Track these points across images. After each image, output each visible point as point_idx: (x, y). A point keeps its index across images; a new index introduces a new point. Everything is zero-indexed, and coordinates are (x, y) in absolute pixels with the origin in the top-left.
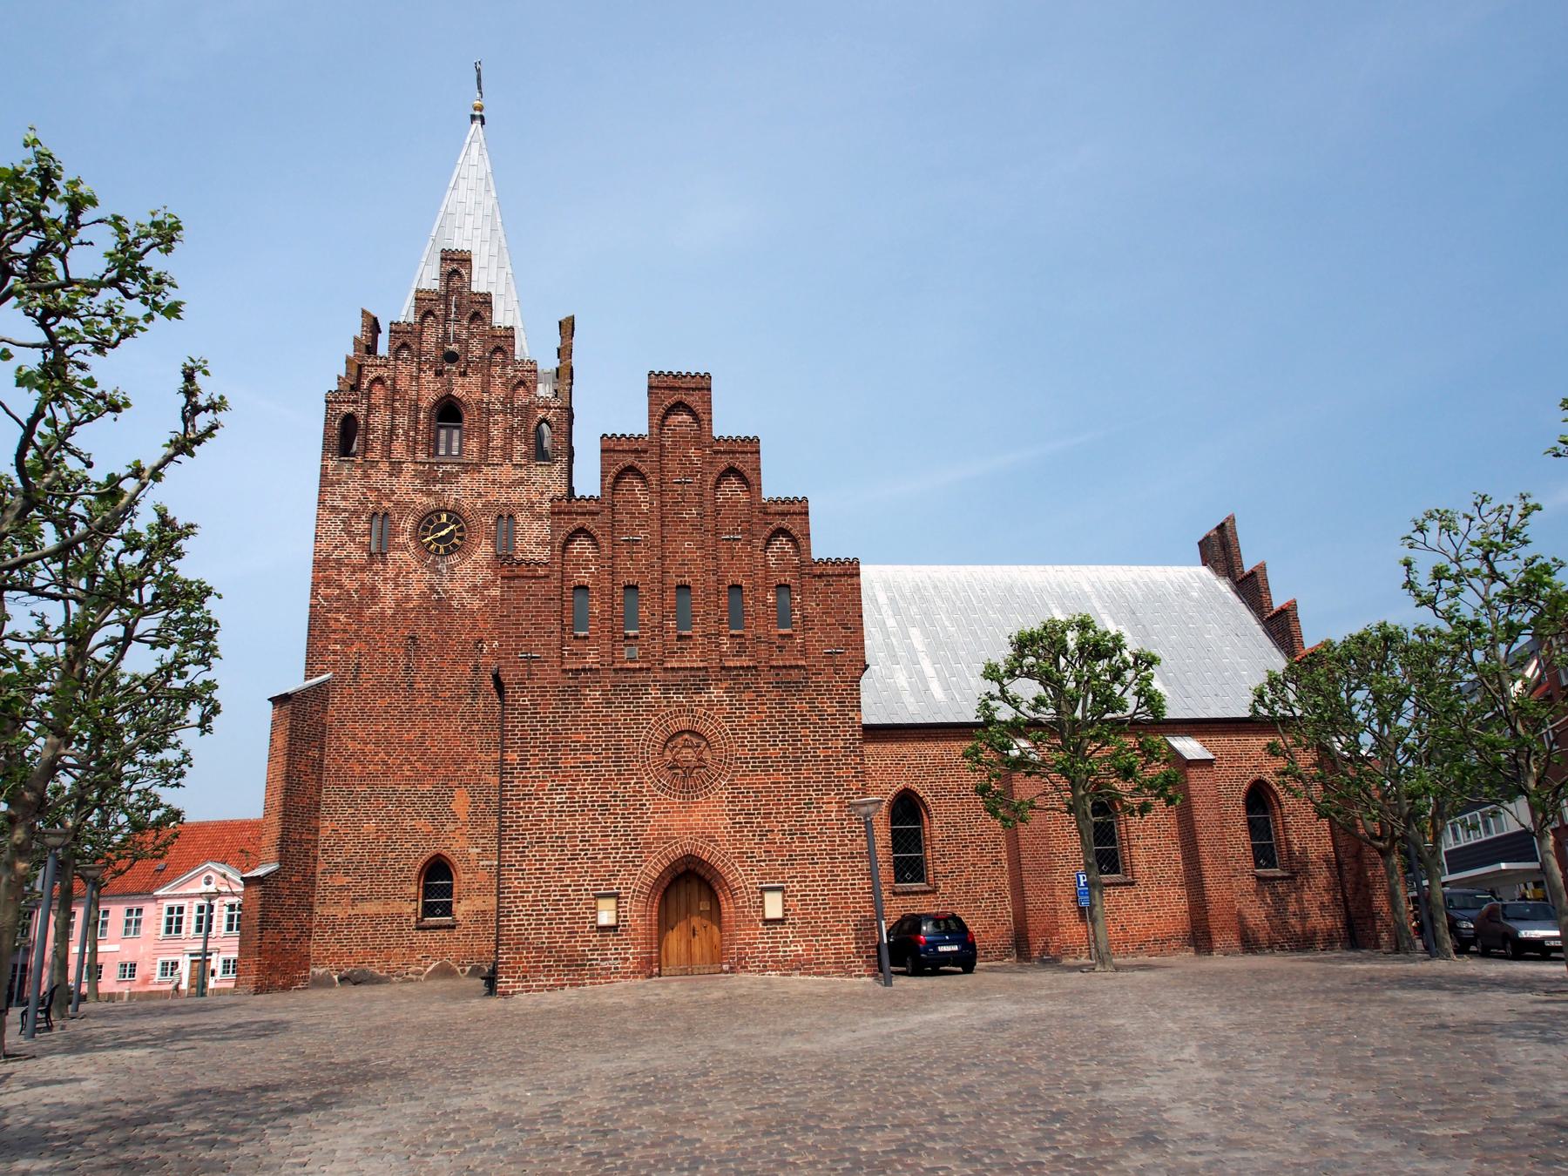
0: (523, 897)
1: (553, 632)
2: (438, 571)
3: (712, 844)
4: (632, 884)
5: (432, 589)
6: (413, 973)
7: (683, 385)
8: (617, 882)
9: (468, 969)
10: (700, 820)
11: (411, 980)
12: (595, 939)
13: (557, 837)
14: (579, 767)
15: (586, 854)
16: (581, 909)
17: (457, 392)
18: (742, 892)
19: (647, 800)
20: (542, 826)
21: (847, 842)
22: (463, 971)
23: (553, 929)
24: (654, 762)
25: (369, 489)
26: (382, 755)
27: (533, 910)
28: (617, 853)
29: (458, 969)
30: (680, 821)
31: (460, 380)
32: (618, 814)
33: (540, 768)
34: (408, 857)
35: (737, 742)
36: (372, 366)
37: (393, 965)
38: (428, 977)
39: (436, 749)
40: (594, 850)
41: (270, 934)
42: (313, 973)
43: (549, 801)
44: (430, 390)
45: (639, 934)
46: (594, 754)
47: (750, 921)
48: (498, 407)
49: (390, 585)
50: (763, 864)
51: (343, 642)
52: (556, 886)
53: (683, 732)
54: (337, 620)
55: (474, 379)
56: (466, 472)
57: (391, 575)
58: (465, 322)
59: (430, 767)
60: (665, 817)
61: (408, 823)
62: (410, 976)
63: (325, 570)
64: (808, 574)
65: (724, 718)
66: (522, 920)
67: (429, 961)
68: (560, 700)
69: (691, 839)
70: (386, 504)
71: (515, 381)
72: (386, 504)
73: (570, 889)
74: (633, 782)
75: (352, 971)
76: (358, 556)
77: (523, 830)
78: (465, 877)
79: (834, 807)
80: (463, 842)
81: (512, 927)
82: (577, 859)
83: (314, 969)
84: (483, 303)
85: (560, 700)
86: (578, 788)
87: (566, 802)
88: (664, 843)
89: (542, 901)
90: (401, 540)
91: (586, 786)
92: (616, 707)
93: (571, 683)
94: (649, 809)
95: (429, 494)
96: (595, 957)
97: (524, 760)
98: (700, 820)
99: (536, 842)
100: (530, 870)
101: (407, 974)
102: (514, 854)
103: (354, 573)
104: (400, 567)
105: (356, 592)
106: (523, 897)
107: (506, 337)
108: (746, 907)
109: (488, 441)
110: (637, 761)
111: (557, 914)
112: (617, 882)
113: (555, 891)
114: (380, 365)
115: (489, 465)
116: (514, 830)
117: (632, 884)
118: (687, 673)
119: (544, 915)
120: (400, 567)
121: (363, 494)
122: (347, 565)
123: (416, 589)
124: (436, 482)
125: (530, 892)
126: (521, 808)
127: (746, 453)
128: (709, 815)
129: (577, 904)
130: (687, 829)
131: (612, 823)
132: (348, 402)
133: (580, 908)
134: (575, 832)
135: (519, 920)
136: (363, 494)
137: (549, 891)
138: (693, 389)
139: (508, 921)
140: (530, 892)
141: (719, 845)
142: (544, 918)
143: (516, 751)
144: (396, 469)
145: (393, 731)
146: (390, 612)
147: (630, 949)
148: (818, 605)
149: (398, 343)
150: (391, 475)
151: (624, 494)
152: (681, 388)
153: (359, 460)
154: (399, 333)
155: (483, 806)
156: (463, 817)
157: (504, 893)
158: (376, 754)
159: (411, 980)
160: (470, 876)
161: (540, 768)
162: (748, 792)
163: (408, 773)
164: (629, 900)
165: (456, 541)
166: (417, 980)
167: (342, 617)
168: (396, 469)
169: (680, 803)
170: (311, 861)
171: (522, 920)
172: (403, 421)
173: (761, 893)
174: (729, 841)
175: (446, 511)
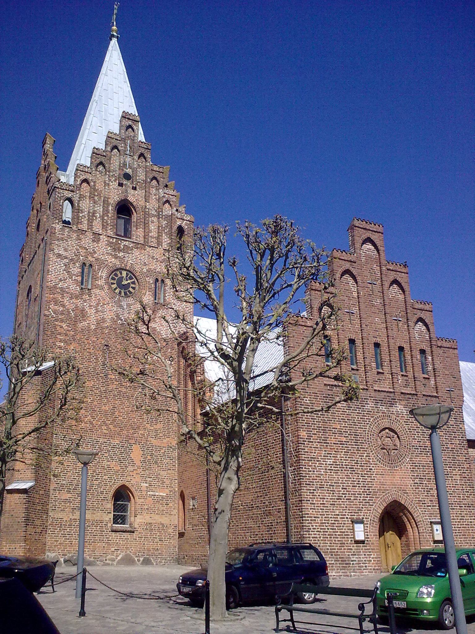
0: (315, 520)
1: (317, 361)
2: (121, 306)
3: (405, 495)
4: (369, 516)
5: (118, 316)
6: (109, 560)
7: (371, 229)
8: (362, 514)
9: (141, 559)
10: (398, 480)
11: (108, 564)
12: (354, 547)
13: (330, 485)
14: (338, 444)
15: (345, 497)
16: (345, 529)
17: (131, 199)
18: (421, 524)
19: (373, 467)
20: (322, 478)
21: (466, 498)
22: (139, 560)
23: (332, 541)
24: (374, 445)
25: (80, 247)
26: (89, 417)
27: (321, 529)
28: (360, 497)
29: (136, 559)
30: (389, 480)
31: (132, 192)
32: (359, 474)
33: (318, 442)
34: (106, 485)
35: (411, 436)
36: (82, 171)
37: (97, 554)
38: (119, 563)
39: (121, 418)
40: (349, 494)
41: (30, 529)
42: (48, 556)
43: (324, 463)
44: (115, 195)
45: (375, 546)
46: (345, 437)
47: (427, 541)
48: (153, 212)
49: (93, 311)
50: (430, 508)
51: (65, 342)
52: (332, 515)
53: (386, 428)
54: (61, 327)
55: (140, 193)
56: (137, 248)
57: (94, 303)
58: (136, 157)
59: (118, 429)
60: (382, 477)
61: (105, 463)
62: (107, 562)
63: (54, 294)
64: (435, 345)
65: (405, 422)
66: (316, 534)
67: (119, 552)
68: (325, 402)
69: (395, 491)
70: (90, 258)
71: (165, 200)
72: (90, 258)
73: (339, 517)
74: (365, 455)
75: (72, 556)
76: (75, 288)
77: (313, 479)
78: (139, 501)
79: (458, 477)
80: (138, 479)
81: (311, 539)
82: (341, 499)
83: (49, 554)
84: (146, 148)
85: (325, 402)
86: (338, 456)
87: (333, 465)
88: (383, 492)
89: (325, 523)
90: (99, 283)
91: (342, 456)
92: (353, 410)
93: (330, 392)
94: (374, 472)
95: (116, 257)
96: (354, 559)
97: (310, 436)
98: (398, 480)
99: (320, 488)
100: (318, 504)
101: (106, 560)
102: (308, 494)
103: (71, 298)
104: (99, 300)
105: (73, 311)
106: (315, 520)
107: (159, 172)
108: (424, 533)
109: (149, 232)
110: (366, 443)
111: (334, 532)
112: (362, 514)
113: (331, 518)
114: (87, 172)
115: (150, 247)
116: (308, 479)
117: (369, 516)
118: (385, 394)
119: (327, 532)
120: (99, 300)
121: (77, 249)
122: (67, 293)
123: (109, 316)
124: (120, 251)
125: (319, 518)
126: (310, 466)
127: (402, 272)
128: (403, 478)
129: (343, 526)
130: (393, 485)
131: (357, 479)
132: (69, 190)
133: (345, 529)
134: (338, 483)
135: (314, 534)
136: (77, 249)
137: (328, 517)
138: (375, 232)
139: (309, 534)
140: (319, 518)
141: (409, 496)
142: (327, 534)
143: (305, 431)
144: (96, 237)
145: (95, 403)
146: (93, 327)
147: (371, 555)
148: (441, 363)
149: (98, 161)
150: (93, 241)
151: (344, 285)
152: (369, 230)
153: (74, 228)
154: (99, 155)
155: (149, 457)
156: (138, 463)
157: (305, 517)
158: (86, 416)
159: (108, 564)
160: (143, 500)
161: (318, 442)
162: (419, 466)
163: (105, 431)
164: (368, 526)
165: (131, 289)
166: (112, 565)
167: (64, 325)
168: (96, 237)
169: (388, 470)
170: (48, 481)
171: (316, 534)
172: (99, 209)
173: (431, 524)
174: (413, 493)
175: (126, 270)
